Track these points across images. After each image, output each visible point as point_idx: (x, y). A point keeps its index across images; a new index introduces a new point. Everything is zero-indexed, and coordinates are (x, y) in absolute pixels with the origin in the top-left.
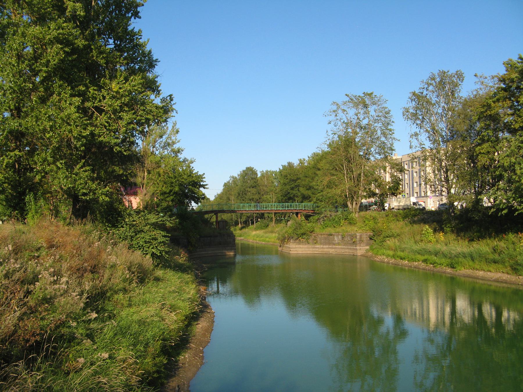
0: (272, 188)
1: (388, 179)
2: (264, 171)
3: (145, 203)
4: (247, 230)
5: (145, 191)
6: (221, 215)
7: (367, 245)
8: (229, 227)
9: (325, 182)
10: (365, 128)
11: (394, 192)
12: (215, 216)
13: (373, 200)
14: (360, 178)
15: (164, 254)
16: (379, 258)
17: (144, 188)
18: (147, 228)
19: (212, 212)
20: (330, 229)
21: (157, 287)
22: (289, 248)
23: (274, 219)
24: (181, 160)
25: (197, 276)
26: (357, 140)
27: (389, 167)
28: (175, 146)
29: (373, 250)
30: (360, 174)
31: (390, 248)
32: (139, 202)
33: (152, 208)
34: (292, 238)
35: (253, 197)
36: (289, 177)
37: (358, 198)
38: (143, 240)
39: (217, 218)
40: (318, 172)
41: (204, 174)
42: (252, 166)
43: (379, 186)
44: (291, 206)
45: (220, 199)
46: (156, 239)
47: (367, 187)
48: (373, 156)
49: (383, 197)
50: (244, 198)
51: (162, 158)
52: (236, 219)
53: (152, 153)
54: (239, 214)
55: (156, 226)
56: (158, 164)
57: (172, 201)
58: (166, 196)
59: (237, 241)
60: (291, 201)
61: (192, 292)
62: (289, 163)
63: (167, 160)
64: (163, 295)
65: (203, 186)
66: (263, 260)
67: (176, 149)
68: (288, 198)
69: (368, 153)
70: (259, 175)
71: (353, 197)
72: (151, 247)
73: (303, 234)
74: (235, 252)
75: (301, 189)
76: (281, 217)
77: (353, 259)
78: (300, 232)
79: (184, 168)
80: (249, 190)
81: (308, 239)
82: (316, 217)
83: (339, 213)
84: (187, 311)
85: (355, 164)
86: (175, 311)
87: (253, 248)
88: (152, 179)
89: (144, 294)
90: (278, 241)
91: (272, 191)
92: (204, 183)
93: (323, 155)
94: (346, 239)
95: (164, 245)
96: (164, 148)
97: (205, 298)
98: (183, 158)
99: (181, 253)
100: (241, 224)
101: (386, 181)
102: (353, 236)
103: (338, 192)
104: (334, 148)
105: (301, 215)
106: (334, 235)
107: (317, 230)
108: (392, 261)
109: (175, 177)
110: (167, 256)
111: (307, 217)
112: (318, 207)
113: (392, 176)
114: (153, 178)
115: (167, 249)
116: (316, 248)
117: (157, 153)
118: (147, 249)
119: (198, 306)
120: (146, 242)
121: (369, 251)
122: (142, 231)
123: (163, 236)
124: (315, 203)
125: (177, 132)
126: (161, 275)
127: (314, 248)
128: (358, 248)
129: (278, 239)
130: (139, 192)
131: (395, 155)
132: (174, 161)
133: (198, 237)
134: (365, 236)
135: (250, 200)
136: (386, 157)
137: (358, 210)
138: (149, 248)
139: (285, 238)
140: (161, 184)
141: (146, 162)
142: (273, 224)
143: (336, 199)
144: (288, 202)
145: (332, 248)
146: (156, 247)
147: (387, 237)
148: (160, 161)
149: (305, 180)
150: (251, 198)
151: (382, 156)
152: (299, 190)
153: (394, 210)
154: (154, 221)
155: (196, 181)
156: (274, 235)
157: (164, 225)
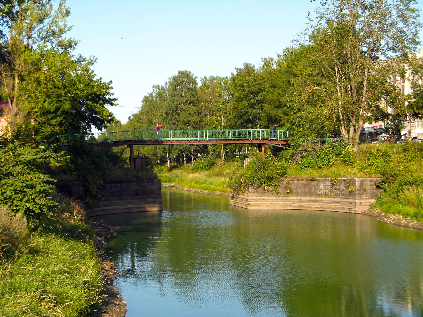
0: (220, 105)
1: (408, 90)
2: (208, 78)
3: (16, 128)
4: (180, 171)
5: (15, 109)
6: (139, 148)
7: (372, 197)
8: (152, 167)
9: (305, 96)
10: (372, 8)
11: (416, 111)
12: (128, 149)
13: (383, 124)
14: (362, 89)
15: (45, 210)
16: (391, 218)
17: (14, 104)
18: (18, 169)
19: (124, 142)
20: (312, 170)
21: (33, 263)
22: (247, 200)
23: (223, 154)
24: (74, 59)
25: (99, 246)
26: (357, 27)
27: (410, 71)
28: (63, 36)
29: (381, 205)
30: (361, 83)
31: (409, 203)
32: (6, 127)
33: (28, 137)
35: (190, 119)
36: (247, 87)
37: (357, 121)
38: (12, 188)
39: (132, 152)
40: (293, 80)
42: (188, 70)
43: (392, 102)
44: (250, 133)
45: (138, 122)
46: (32, 187)
47: (374, 104)
48: (384, 54)
49: (399, 119)
50: (175, 121)
51: (42, 56)
53: (27, 47)
54: (167, 147)
55: (33, 165)
56: (36, 65)
57: (60, 124)
58: (50, 116)
59: (163, 190)
60: (250, 125)
61: (91, 271)
62: (247, 65)
63: (52, 59)
64: (44, 278)
65: (110, 102)
66: (205, 219)
67: (66, 42)
68: (245, 120)
69: (375, 49)
70: (200, 84)
71: (349, 120)
72: (26, 199)
73: (269, 178)
74: (161, 207)
75: (266, 107)
76: (232, 152)
77: (349, 218)
79: (79, 72)
80: (184, 107)
81: (277, 186)
82: (290, 151)
83: (327, 145)
84: (82, 302)
85: (354, 66)
86: (62, 303)
87: (189, 200)
88: (27, 90)
89: (11, 276)
90: (228, 190)
91: (219, 109)
92: (112, 97)
93: (302, 53)
94: (338, 187)
95: (46, 196)
96: (46, 39)
97: (112, 281)
98: (77, 56)
99: (74, 208)
100: (170, 161)
101: (403, 95)
102: (349, 183)
103: (326, 111)
104: (320, 40)
105: (266, 149)
106: (318, 181)
107: (291, 172)
108: (414, 223)
109: (65, 87)
110: (51, 214)
111: (276, 151)
112: (293, 135)
113: (415, 85)
114: (29, 87)
115: (50, 203)
116: (290, 201)
117: (35, 47)
118: (19, 203)
119: (100, 295)
120: (16, 192)
121: (375, 207)
122: (10, 174)
123: (44, 182)
124: (289, 129)
125: (68, 13)
126: (41, 245)
127: (286, 201)
128: (357, 201)
129: (230, 186)
130: (6, 109)
131: (419, 52)
132: (63, 61)
133: (102, 182)
135: (185, 123)
136: (405, 55)
137: (357, 141)
138: (21, 200)
140: (42, 97)
141: (17, 62)
142: (221, 162)
143: (322, 123)
144: (244, 127)
145: (315, 201)
146: (33, 199)
147: (406, 184)
148: (40, 60)
149: (272, 93)
150: (186, 120)
151: (399, 53)
152: (262, 109)
153: (417, 141)
154: (29, 157)
155: (98, 93)
156: (222, 179)
157: (47, 164)
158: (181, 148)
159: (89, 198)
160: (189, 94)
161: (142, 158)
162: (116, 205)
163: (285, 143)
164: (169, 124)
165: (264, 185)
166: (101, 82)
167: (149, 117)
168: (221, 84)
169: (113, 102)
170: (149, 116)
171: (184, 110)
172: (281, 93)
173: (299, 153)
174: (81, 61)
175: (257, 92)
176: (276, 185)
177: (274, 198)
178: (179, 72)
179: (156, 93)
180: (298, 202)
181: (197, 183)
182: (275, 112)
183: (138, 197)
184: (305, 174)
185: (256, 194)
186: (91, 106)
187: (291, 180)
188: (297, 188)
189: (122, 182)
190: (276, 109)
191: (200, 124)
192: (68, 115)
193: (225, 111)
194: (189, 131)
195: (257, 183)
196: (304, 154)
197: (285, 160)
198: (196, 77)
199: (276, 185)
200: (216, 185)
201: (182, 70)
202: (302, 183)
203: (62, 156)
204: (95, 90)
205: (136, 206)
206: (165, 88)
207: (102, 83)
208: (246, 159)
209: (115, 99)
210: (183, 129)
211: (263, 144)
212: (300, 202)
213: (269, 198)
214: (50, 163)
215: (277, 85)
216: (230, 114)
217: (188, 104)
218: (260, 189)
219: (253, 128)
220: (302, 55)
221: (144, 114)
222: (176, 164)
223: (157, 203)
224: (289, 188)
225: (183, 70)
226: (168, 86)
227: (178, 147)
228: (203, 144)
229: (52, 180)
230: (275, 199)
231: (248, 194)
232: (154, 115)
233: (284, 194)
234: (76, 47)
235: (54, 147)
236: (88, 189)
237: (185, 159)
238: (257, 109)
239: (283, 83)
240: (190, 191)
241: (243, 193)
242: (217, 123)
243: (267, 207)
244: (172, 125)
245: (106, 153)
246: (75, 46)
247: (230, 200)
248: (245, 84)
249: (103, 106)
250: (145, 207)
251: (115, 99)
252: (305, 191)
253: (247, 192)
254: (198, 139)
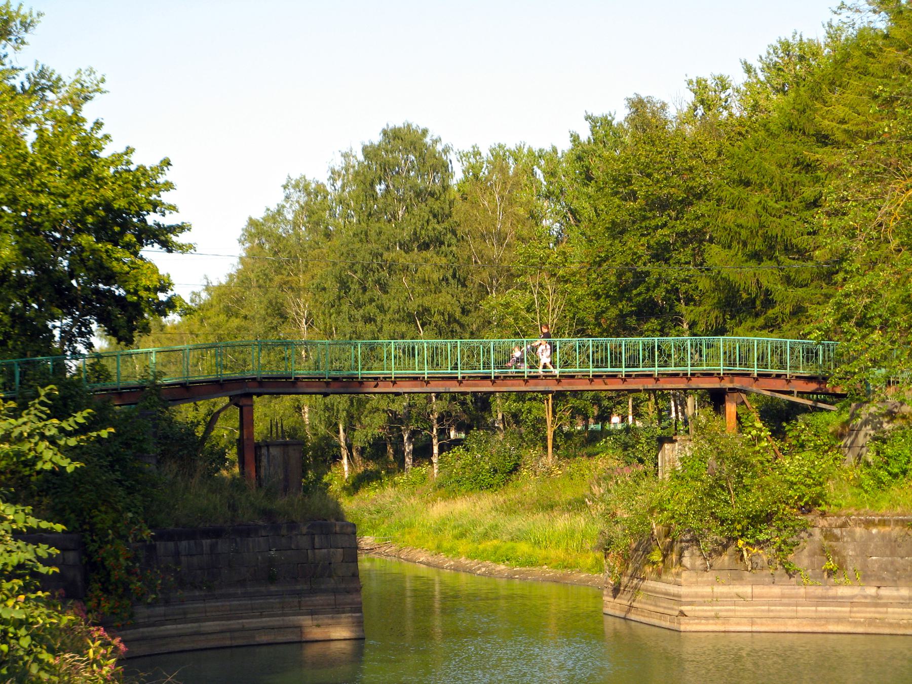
2: (485, 153)
4: (390, 491)
19: (217, 386)
22: (677, 599)
24: (18, 81)
34: (695, 541)
35: (427, 301)
36: (641, 187)
40: (824, 156)
41: (167, 163)
42: (418, 122)
45: (229, 312)
50: (371, 309)
52: (322, 429)
59: (364, 563)
60: (654, 323)
62: (638, 105)
65: (162, 237)
68: (639, 306)
70: (458, 174)
75: (715, 254)
76: (584, 423)
78: (735, 506)
82: (832, 418)
87: (453, 600)
92: (168, 220)
98: (31, 69)
100: (350, 457)
107: (840, 495)
111: (778, 416)
123: (17, 535)
127: (823, 600)
133: (148, 533)
135: (410, 318)
139: (645, 545)
144: (632, 331)
150: (413, 306)
158: (395, 407)
159: (99, 593)
160: (421, 210)
161: (285, 445)
162: (197, 620)
163: (813, 386)
164: (351, 318)
165: (741, 543)
166: (129, 163)
167: (270, 296)
168: (533, 174)
169: (174, 238)
170: (274, 292)
171: (406, 269)
172: (771, 203)
173: (866, 423)
174: (43, 89)
175: (681, 202)
176: (784, 542)
177: (776, 590)
178: (385, 133)
179: (297, 206)
180: (866, 605)
181: (462, 535)
182: (746, 275)
183: (273, 588)
184: (894, 503)
185: (709, 576)
186: (94, 251)
187: (839, 522)
188: (864, 553)
189: (217, 533)
190: (753, 263)
191: (465, 320)
192: (10, 287)
193: (561, 272)
194: (425, 342)
195: (715, 536)
196: (887, 426)
197: (816, 448)
198: (446, 151)
199: (784, 542)
200: (537, 543)
201: (397, 122)
202: (883, 537)
203: (82, 429)
204: (110, 194)
205: (266, 621)
206: (329, 188)
207: (133, 168)
208: (667, 446)
209: (182, 228)
210: (403, 338)
211: (733, 390)
212: (876, 605)
213: (758, 590)
214: (38, 457)
215: (753, 177)
216: (576, 284)
217: (420, 248)
218: (725, 558)
219: (663, 333)
220: (848, 65)
221: (254, 284)
222: (372, 466)
223: (344, 612)
224: (835, 553)
225: (399, 124)
226: (339, 184)
227: (383, 405)
228: (474, 394)
229: (44, 525)
230: (783, 596)
231: (678, 574)
232: (292, 288)
233: (814, 577)
234: (27, 37)
235: (48, 395)
236: (96, 558)
237: (408, 448)
238: (678, 262)
239: (780, 166)
240: (439, 567)
241: (659, 574)
242: (529, 316)
243: (752, 624)
244: (360, 324)
245: (155, 426)
246: (23, 34)
247: (606, 599)
248: (636, 174)
249: (135, 254)
250: (300, 627)
251: (182, 228)
252: (892, 563)
253: (674, 571)
254: (459, 374)
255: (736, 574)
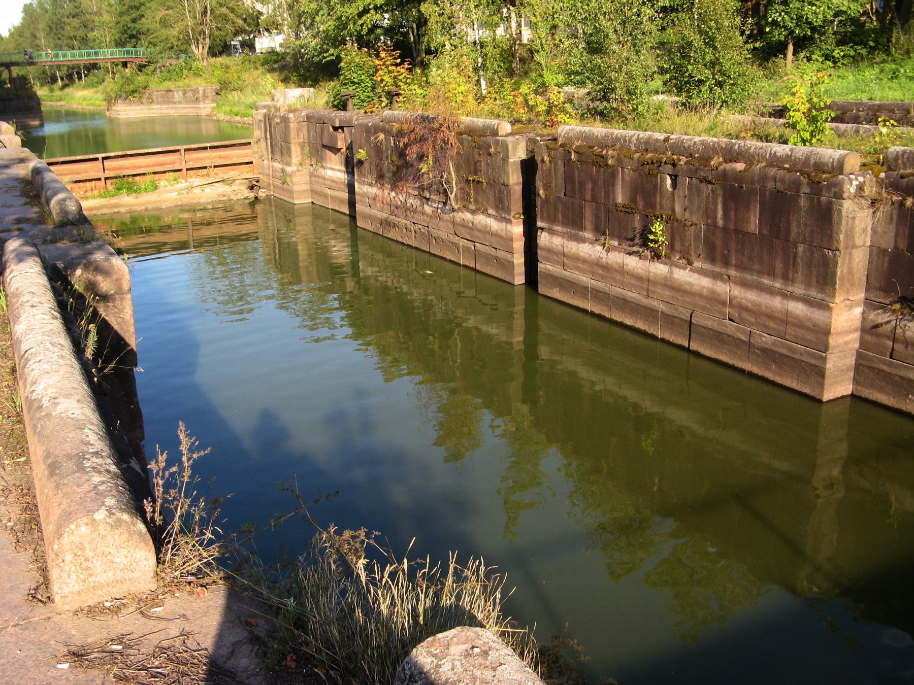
45: (20, 36)
50: (60, 36)
71: (198, 40)
73: (133, 92)
77: (197, 120)
80: (67, 20)
82: (152, 67)
83: (181, 60)
102: (195, 91)
107: (153, 86)
127: (149, 109)
134: (209, 91)
137: (206, 56)
150: (71, 35)
188: (157, 98)
189: (4, 100)
195: (124, 95)
222: (67, 82)
255: (130, 103)
